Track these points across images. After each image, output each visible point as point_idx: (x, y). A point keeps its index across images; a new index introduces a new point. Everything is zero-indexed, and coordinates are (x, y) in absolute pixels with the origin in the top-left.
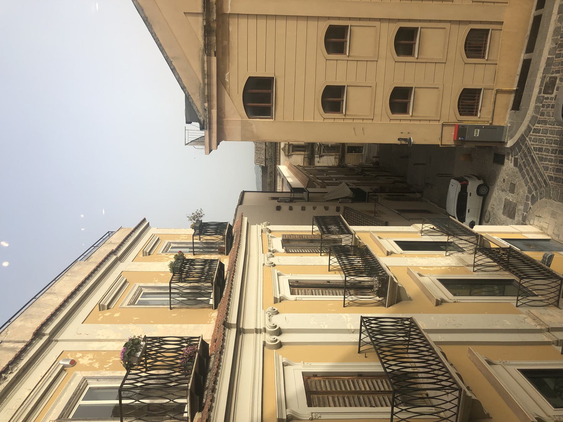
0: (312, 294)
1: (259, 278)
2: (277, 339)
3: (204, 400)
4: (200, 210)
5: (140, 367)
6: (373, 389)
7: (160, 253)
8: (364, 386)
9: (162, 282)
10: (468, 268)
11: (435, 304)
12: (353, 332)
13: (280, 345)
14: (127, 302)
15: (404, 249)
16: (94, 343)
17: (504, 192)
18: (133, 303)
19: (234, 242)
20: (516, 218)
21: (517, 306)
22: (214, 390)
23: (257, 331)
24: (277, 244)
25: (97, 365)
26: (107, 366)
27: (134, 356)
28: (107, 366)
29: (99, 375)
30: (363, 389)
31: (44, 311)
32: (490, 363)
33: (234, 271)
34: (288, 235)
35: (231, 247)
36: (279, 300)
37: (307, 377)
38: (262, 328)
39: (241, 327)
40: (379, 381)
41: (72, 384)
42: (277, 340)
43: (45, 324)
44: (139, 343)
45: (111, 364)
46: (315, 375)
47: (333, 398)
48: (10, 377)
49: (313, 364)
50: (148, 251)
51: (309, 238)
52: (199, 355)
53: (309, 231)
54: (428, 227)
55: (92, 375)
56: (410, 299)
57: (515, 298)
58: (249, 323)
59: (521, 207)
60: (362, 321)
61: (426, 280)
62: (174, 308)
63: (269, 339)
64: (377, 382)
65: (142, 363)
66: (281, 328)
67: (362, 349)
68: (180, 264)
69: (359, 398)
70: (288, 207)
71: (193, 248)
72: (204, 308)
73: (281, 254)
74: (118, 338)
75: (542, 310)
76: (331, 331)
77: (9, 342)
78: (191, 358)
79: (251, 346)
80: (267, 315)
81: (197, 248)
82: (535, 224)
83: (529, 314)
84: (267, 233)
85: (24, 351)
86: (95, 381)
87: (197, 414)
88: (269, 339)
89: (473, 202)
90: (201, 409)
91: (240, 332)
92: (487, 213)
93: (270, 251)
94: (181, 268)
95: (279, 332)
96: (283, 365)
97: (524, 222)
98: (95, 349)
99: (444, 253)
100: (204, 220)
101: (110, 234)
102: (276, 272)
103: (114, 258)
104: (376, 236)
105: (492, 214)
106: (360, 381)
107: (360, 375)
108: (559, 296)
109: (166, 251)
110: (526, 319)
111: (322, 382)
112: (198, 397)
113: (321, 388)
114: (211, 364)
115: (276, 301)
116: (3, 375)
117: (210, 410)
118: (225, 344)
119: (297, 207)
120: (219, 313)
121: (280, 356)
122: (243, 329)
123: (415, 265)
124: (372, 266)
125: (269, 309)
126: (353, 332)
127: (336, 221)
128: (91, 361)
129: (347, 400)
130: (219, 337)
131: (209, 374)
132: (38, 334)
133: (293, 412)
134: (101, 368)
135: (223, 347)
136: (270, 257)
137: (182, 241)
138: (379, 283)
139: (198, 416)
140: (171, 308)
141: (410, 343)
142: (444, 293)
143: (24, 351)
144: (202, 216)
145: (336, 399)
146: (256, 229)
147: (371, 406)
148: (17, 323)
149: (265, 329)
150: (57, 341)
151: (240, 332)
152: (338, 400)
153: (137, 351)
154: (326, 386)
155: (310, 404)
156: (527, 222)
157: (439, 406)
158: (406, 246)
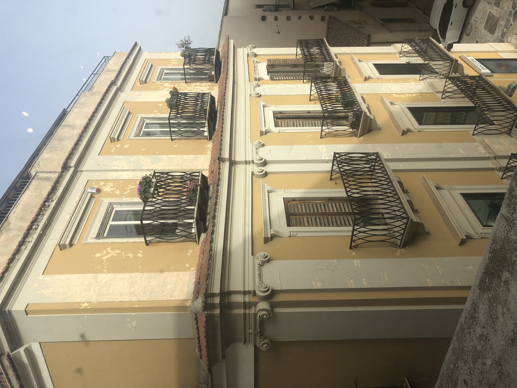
0: (294, 126)
1: (247, 110)
2: (263, 170)
3: (207, 223)
4: (187, 37)
5: (154, 200)
6: (340, 211)
7: (155, 81)
8: (332, 208)
9: (161, 113)
10: (437, 94)
11: (401, 134)
12: (327, 162)
13: (266, 174)
14: (133, 133)
15: (381, 73)
16: (112, 173)
17: (490, 5)
18: (138, 135)
19: (222, 70)
20: (496, 34)
21: (473, 135)
22: (214, 217)
23: (246, 162)
24: (262, 70)
25: (118, 192)
26: (126, 193)
27: (149, 192)
28: (126, 193)
29: (121, 201)
30: (332, 211)
31: (65, 143)
32: (438, 188)
33: (224, 105)
34: (273, 60)
35: (220, 75)
36: (264, 133)
37: (287, 201)
38: (250, 160)
39: (233, 159)
40: (345, 204)
41: (101, 208)
42: (263, 171)
43: (69, 158)
44: (151, 181)
45: (129, 191)
46: (294, 200)
47: (307, 218)
48: (53, 204)
49: (293, 191)
50: (144, 80)
51: (293, 63)
52: (200, 188)
53: (293, 54)
54: (407, 47)
55: (116, 201)
56: (380, 129)
57: (474, 126)
58: (239, 156)
59: (503, 23)
60: (335, 156)
61: (395, 108)
62: (175, 139)
63: (257, 169)
64: (343, 205)
65: (155, 196)
66: (267, 160)
67: (333, 177)
68: (175, 100)
69: (328, 218)
70: (273, 17)
71: (185, 74)
72: (200, 139)
73: (266, 83)
74: (131, 169)
75: (494, 138)
76: (309, 158)
77: (43, 172)
78: (194, 191)
79: (242, 174)
80: (254, 148)
81: (190, 74)
82: (512, 41)
83: (482, 142)
84: (253, 58)
85: (57, 182)
86: (119, 206)
87: (202, 234)
88: (257, 169)
89: (457, 14)
90: (205, 230)
91: (232, 163)
92: (469, 26)
93: (256, 79)
94: (176, 101)
95: (265, 163)
96: (268, 192)
97: (501, 40)
98: (114, 178)
99: (417, 76)
100: (193, 46)
101: (106, 59)
102: (262, 103)
103: (114, 88)
104: (356, 58)
105: (474, 27)
106: (330, 204)
107: (330, 199)
108: (513, 125)
109: (160, 79)
110: (478, 148)
111: (299, 205)
112: (202, 223)
113: (298, 210)
114: (210, 192)
115: (262, 133)
116: (47, 204)
117: (212, 234)
118: (220, 176)
119: (282, 16)
120: (213, 144)
121: (266, 185)
122: (235, 161)
123: (389, 92)
124: (349, 100)
125: (256, 143)
126: (327, 162)
127: (319, 43)
128: (112, 189)
129: (318, 220)
130: (215, 169)
131: (209, 201)
132: (65, 167)
133: (276, 231)
134: (121, 195)
135: (219, 179)
136: (256, 87)
137: (174, 67)
138: (353, 117)
139: (203, 236)
140: (172, 140)
141: (373, 177)
142: (411, 122)
143: (57, 182)
144: (190, 43)
145: (310, 219)
146: (242, 53)
147: (337, 226)
148: (45, 155)
149: (254, 292)
150: (82, 171)
151: (233, 164)
152: (311, 220)
153: (150, 187)
154: (301, 208)
155: (289, 225)
156: (505, 39)
157: (392, 224)
158: (384, 69)
